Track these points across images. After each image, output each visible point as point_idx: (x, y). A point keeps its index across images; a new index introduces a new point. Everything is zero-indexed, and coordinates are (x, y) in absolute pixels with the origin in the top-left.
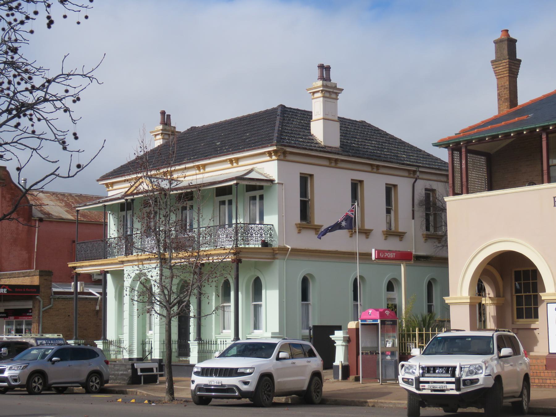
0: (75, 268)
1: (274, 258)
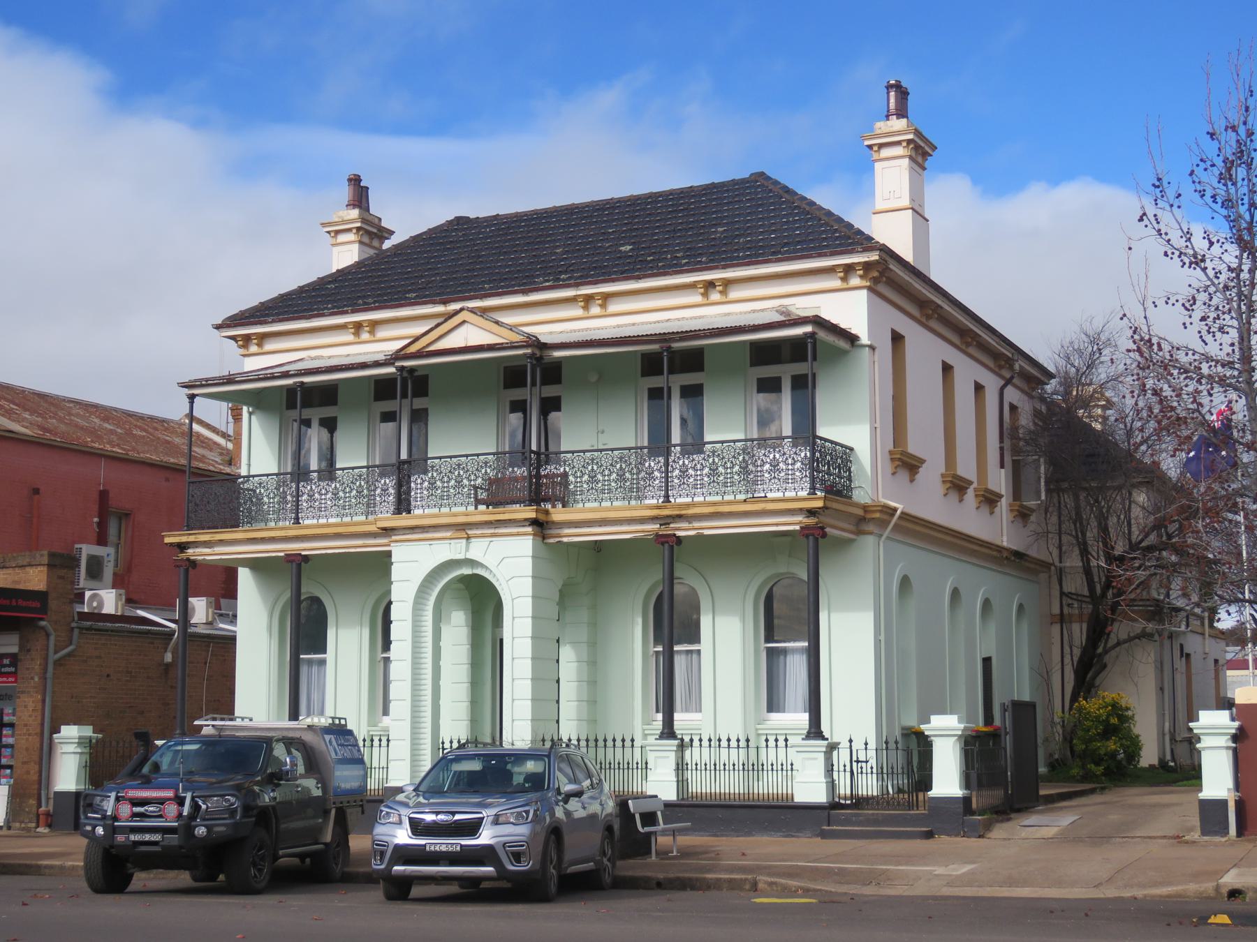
0: (182, 547)
1: (860, 532)
